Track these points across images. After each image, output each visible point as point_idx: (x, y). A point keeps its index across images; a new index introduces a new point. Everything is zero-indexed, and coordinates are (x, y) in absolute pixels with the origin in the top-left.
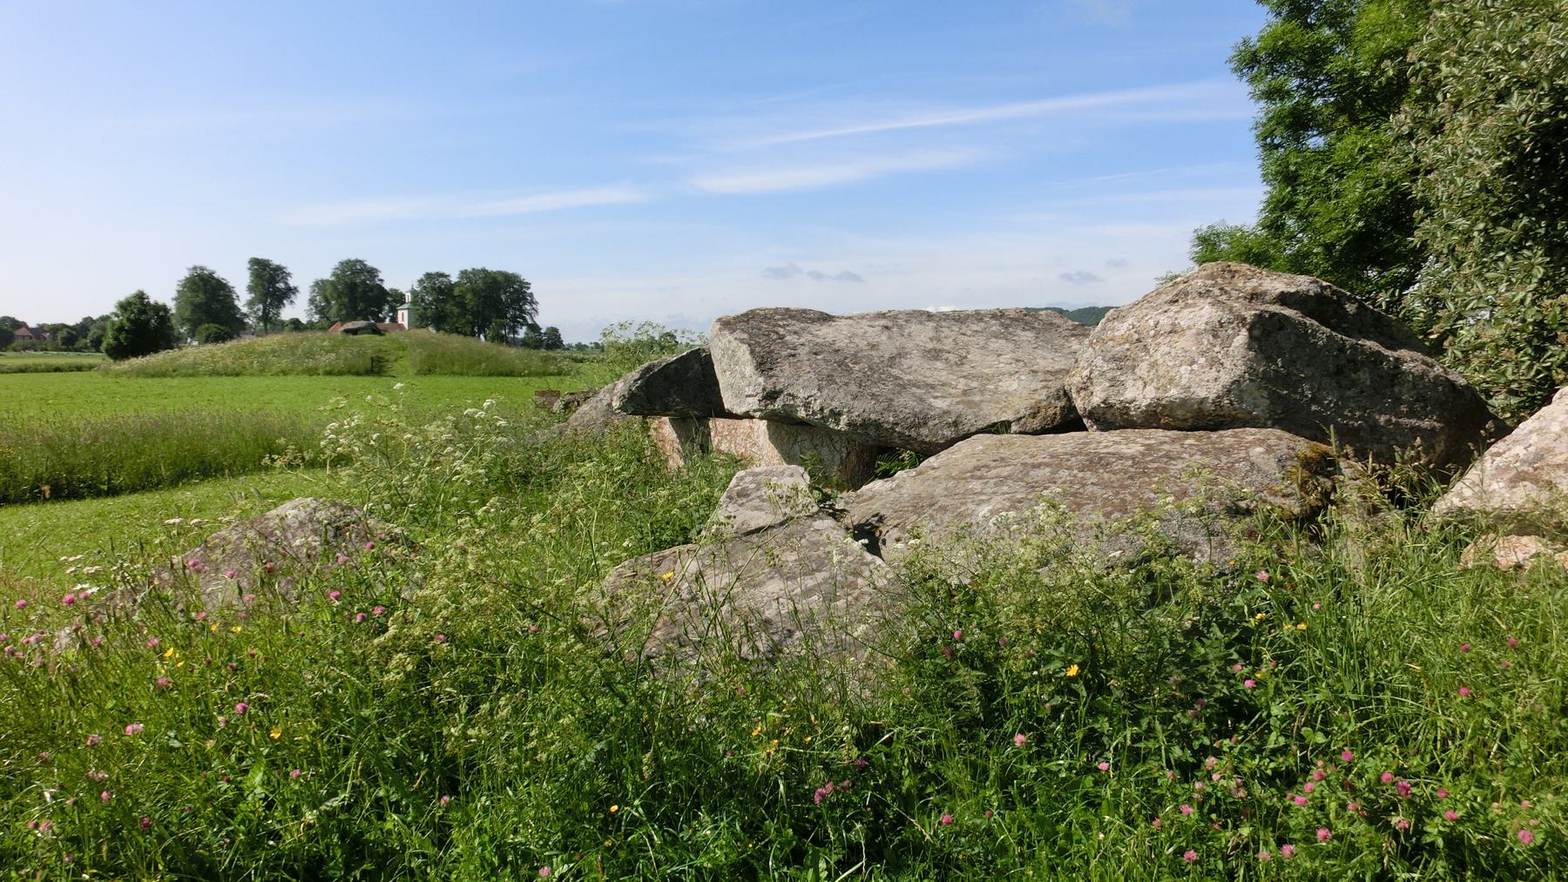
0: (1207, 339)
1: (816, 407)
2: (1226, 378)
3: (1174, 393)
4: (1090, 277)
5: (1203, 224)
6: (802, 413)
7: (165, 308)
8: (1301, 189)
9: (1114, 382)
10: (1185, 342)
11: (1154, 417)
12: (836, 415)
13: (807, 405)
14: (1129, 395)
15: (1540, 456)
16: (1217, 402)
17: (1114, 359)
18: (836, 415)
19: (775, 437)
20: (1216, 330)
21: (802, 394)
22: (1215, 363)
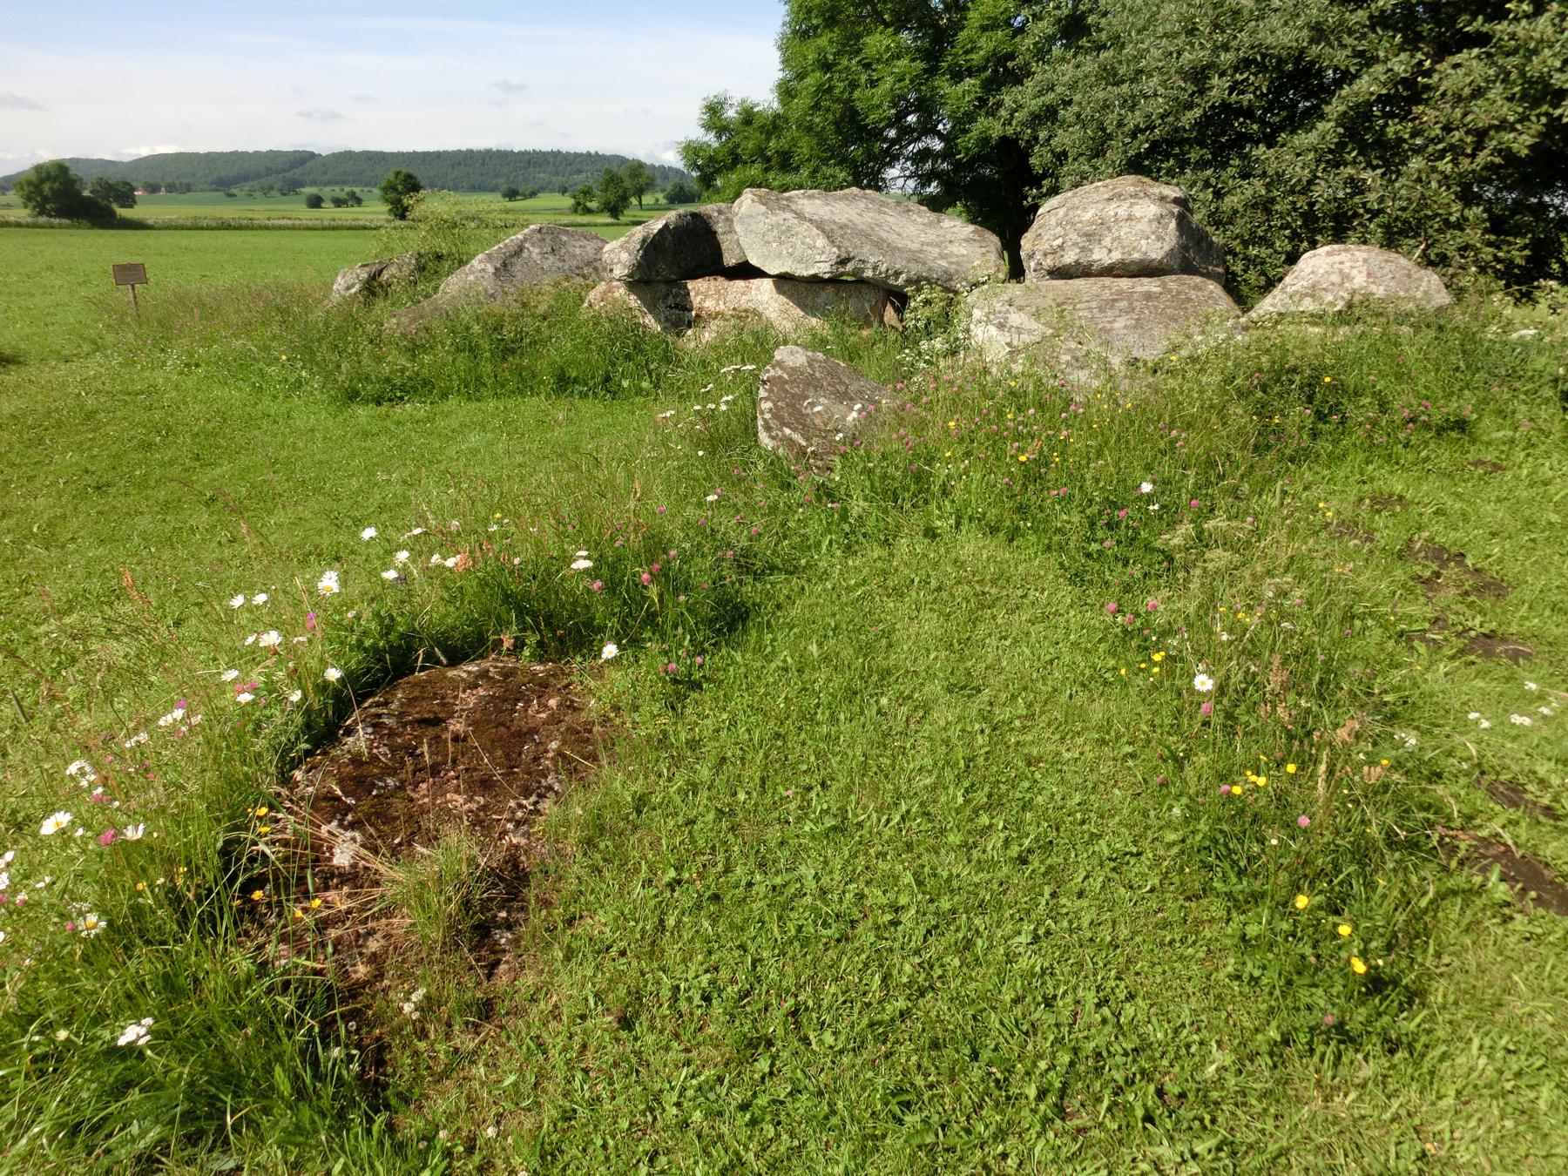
0: (1154, 225)
1: (883, 269)
2: (1167, 248)
3: (1136, 256)
4: (335, 116)
5: (713, 90)
6: (869, 274)
7: (678, 171)
8: (837, 76)
9: (1083, 249)
10: (1142, 226)
11: (1110, 271)
12: (897, 274)
13: (875, 268)
14: (1095, 257)
15: (1314, 286)
16: (1160, 262)
17: (1086, 235)
18: (897, 274)
19: (779, 290)
20: (1159, 219)
21: (872, 260)
22: (1159, 238)
